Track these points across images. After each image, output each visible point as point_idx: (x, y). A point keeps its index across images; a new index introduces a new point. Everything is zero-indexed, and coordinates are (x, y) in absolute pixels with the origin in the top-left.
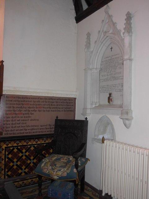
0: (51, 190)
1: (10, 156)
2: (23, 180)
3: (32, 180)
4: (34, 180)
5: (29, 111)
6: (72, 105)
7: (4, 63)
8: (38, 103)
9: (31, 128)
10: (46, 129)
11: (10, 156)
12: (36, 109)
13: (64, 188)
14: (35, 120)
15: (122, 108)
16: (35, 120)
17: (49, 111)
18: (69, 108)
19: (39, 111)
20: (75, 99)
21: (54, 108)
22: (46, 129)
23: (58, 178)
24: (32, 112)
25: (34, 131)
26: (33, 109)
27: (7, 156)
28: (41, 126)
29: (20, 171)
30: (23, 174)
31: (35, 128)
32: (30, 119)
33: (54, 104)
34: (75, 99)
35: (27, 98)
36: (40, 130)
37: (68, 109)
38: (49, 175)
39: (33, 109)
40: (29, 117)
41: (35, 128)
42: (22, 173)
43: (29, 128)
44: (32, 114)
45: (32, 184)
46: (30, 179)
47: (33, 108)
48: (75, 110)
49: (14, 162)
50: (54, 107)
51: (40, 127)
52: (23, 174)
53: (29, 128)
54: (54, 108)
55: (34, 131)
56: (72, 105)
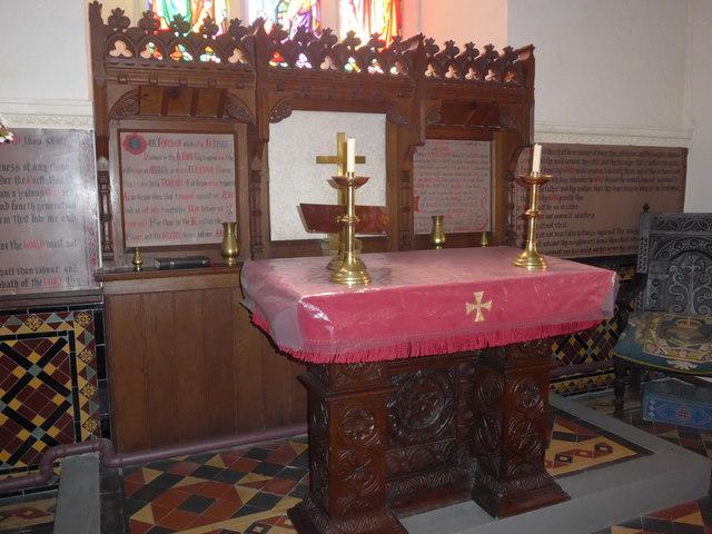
0: (653, 402)
1: (59, 399)
2: (589, 373)
3: (572, 383)
4: (576, 382)
5: (573, 189)
6: (678, 172)
7: (535, 52)
8: (594, 167)
9: (577, 238)
10: (612, 241)
11: (59, 399)
12: (588, 185)
13: (247, 494)
14: (587, 215)
15: (480, 235)
16: (587, 215)
17: (618, 189)
18: (668, 180)
19: (595, 188)
20: (685, 152)
21: (632, 180)
22: (612, 241)
23: (695, 366)
24: (581, 193)
25: (584, 246)
26: (581, 185)
27: (70, 399)
28: (601, 233)
29: (582, 352)
30: (589, 360)
31: (587, 238)
32: (575, 212)
33: (632, 168)
34: (685, 152)
35: (569, 152)
36: (596, 246)
37: (666, 184)
38: (664, 361)
39: (581, 185)
40: (573, 207)
41: (587, 238)
42: (586, 357)
43: (572, 239)
44: (580, 198)
45: (572, 395)
46: (568, 379)
47: (582, 180)
48: (684, 187)
49: (35, 427)
50: (631, 176)
51: (597, 237)
52: (589, 360)
53: (572, 239)
54: (632, 180)
55: (584, 246)
56: (678, 172)
